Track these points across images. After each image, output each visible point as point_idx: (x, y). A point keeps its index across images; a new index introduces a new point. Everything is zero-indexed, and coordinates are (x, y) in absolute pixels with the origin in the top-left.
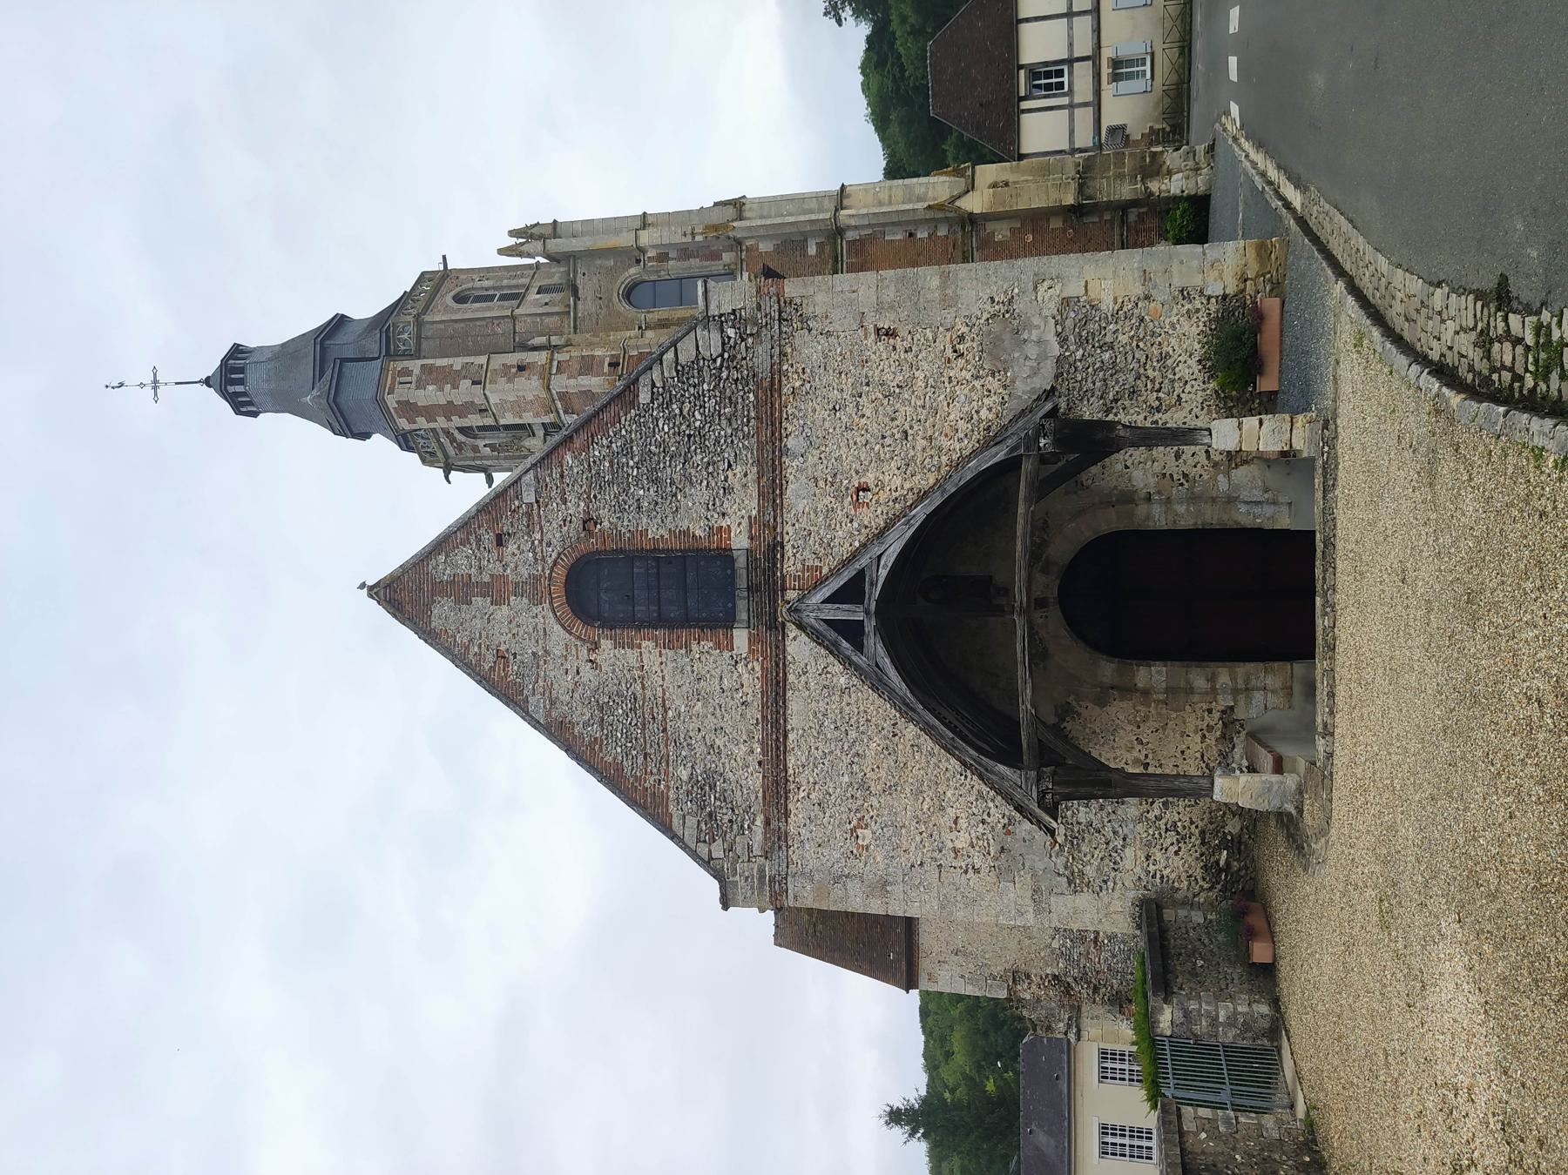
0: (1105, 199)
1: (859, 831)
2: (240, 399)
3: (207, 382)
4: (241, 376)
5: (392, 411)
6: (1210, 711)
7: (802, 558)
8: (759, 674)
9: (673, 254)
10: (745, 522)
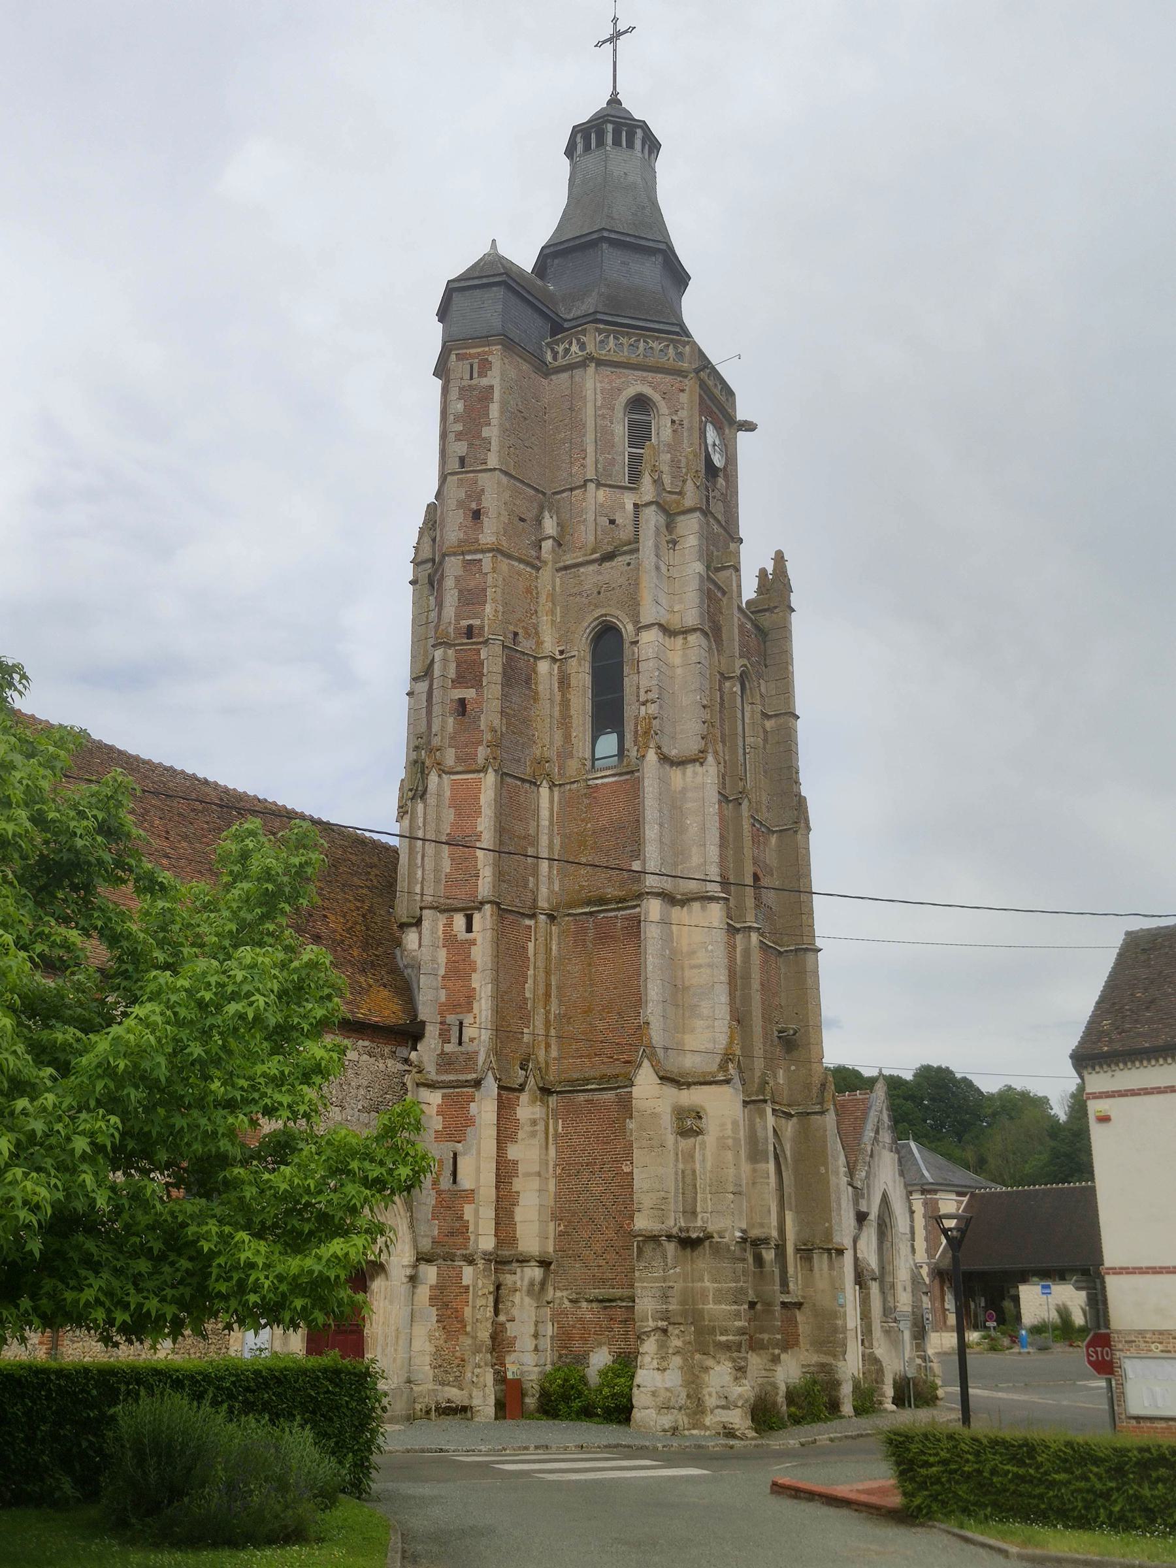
2: (593, 136)
3: (614, 101)
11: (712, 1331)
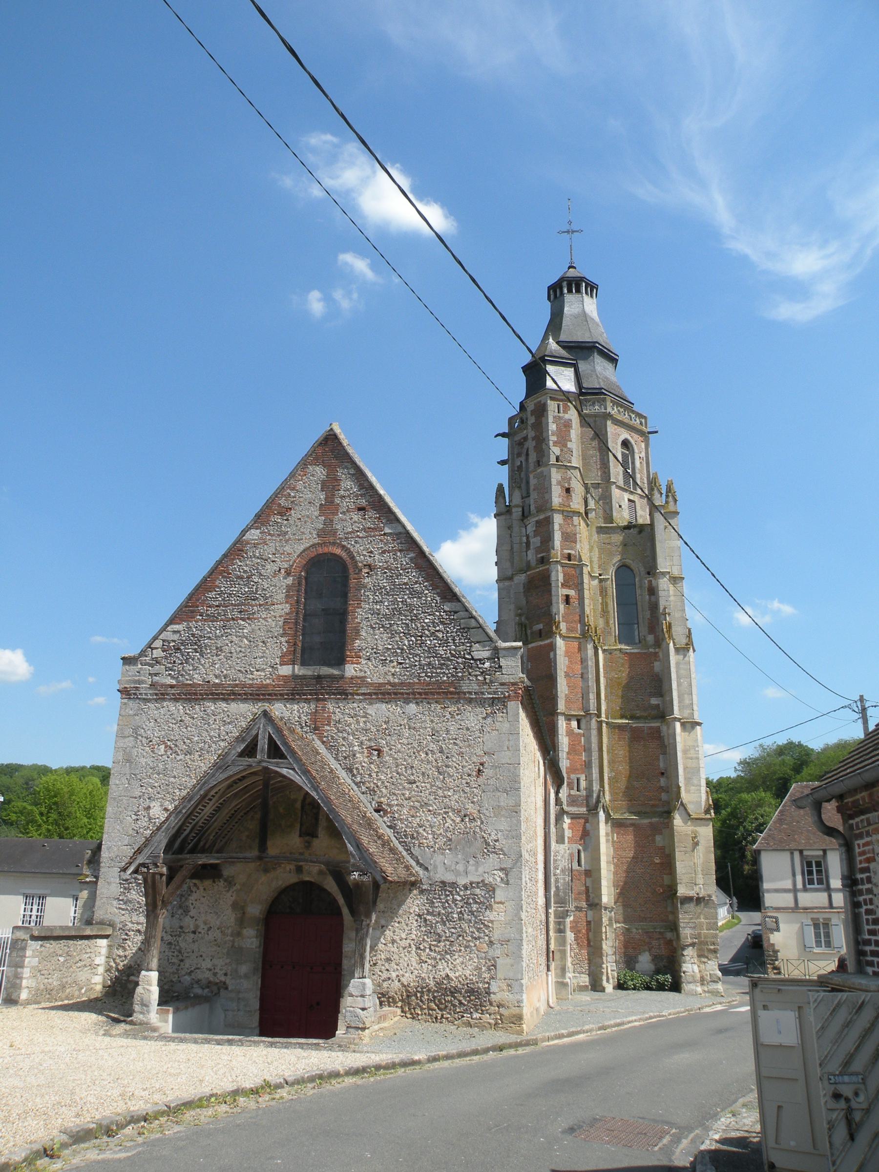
0: (680, 916)
1: (163, 747)
4: (574, 291)
5: (539, 399)
6: (226, 974)
7: (337, 712)
8: (264, 683)
9: (653, 598)
10: (362, 674)
11: (706, 943)
